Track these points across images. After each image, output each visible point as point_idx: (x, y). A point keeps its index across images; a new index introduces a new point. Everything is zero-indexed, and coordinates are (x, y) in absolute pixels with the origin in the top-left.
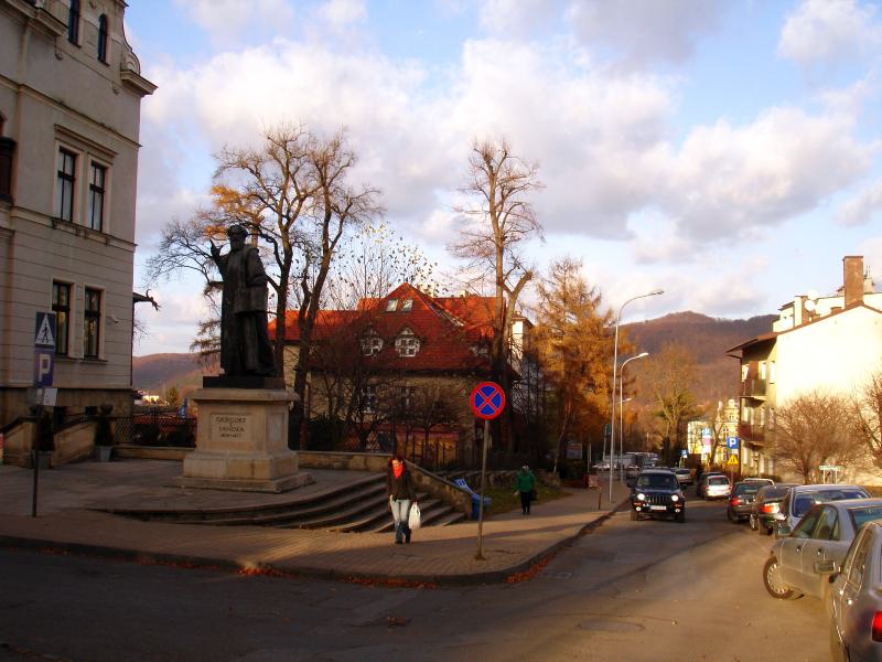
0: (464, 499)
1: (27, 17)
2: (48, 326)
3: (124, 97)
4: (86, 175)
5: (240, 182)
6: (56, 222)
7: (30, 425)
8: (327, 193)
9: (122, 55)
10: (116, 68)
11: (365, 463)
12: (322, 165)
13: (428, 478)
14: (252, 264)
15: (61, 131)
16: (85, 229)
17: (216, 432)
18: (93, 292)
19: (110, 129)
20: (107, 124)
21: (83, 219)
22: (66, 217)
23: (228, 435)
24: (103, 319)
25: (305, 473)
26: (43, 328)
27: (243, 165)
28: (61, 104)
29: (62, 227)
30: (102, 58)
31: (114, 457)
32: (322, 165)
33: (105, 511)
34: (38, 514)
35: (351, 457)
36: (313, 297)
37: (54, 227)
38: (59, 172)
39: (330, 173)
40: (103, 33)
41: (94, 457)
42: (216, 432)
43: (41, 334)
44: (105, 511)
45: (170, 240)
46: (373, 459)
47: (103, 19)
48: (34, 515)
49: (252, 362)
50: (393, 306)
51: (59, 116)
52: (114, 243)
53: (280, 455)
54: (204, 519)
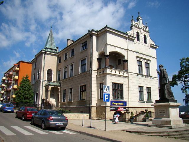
2: (107, 89)
6: (137, 74)
15: (137, 57)
19: (149, 56)
22: (141, 73)
23: (161, 114)
26: (106, 89)
33: (124, 131)
48: (83, 125)
49: (167, 96)
52: (152, 78)
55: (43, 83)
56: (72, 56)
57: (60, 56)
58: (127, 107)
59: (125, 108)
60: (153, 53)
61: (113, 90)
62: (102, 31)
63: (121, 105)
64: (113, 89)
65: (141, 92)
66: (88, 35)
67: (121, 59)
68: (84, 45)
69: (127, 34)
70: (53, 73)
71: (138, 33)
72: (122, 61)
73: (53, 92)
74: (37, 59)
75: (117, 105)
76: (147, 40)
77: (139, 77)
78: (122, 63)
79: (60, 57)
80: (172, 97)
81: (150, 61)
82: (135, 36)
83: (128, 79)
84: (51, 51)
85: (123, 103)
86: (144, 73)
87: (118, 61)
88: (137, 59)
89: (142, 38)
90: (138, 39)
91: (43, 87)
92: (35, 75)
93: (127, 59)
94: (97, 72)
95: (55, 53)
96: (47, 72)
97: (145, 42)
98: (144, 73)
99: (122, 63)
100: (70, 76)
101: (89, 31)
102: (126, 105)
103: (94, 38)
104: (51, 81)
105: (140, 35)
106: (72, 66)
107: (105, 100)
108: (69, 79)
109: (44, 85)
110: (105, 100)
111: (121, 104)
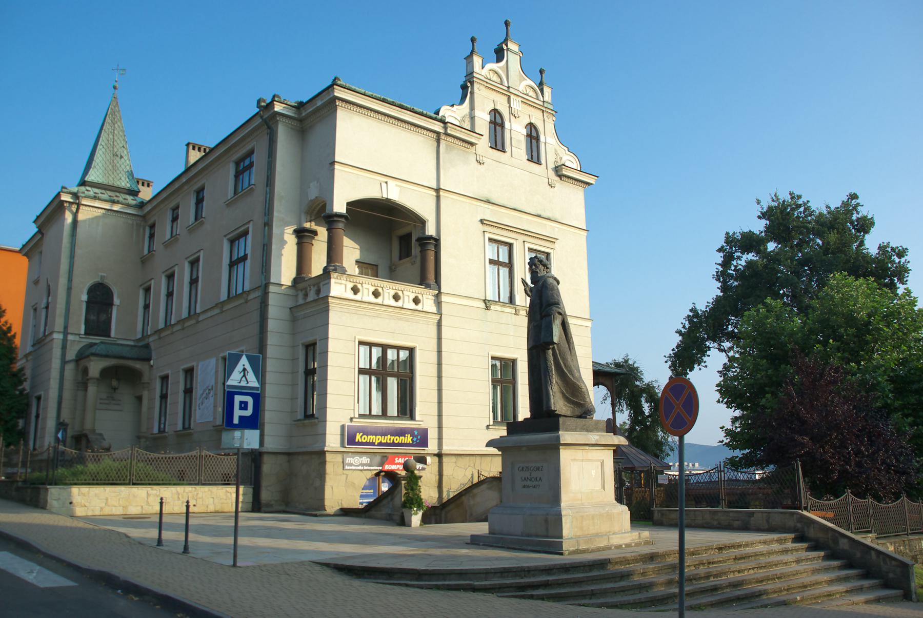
1: (438, 133)
11: (768, 521)
13: (846, 541)
22: (505, 297)
23: (528, 487)
26: (239, 367)
29: (498, 308)
34: (238, 564)
37: (487, 308)
48: (235, 565)
51: (488, 212)
55: (64, 348)
56: (196, 219)
57: (150, 222)
60: (571, 203)
61: (495, 388)
64: (493, 381)
66: (259, 121)
69: (443, 122)
70: (116, 301)
74: (43, 234)
75: (380, 444)
81: (552, 240)
85: (413, 435)
87: (399, 241)
90: (498, 143)
91: (64, 362)
92: (35, 310)
94: (589, 324)
96: (85, 297)
97: (534, 156)
99: (415, 250)
100: (185, 314)
101: (259, 101)
103: (283, 135)
104: (109, 336)
106: (194, 263)
107: (236, 421)
108: (183, 329)
109: (71, 355)
110: (236, 421)
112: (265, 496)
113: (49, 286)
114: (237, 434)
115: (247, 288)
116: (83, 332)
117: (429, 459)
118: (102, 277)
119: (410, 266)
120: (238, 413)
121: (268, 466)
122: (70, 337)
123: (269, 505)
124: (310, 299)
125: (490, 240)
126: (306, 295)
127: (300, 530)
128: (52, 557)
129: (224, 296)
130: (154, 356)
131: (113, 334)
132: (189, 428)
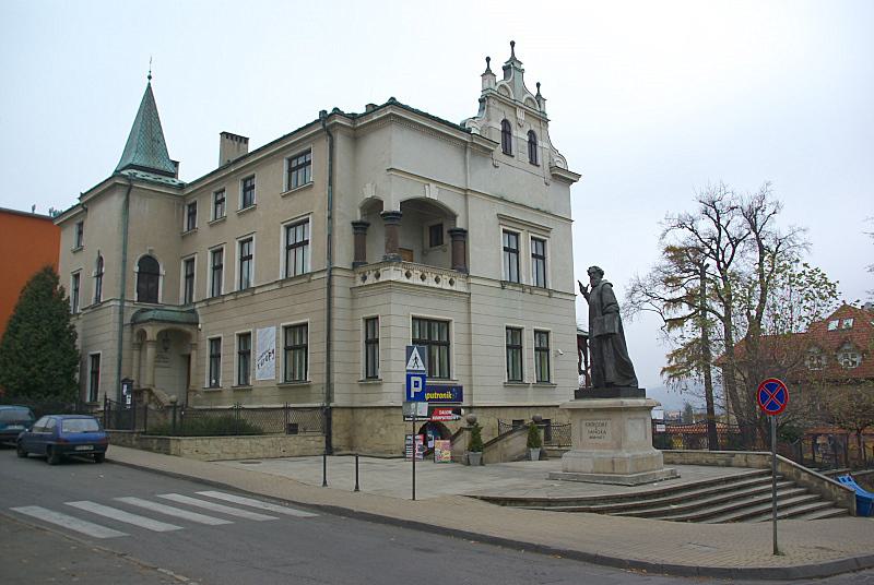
0: (845, 495)
2: (418, 356)
3: (555, 187)
4: (526, 248)
5: (680, 238)
6: (503, 284)
7: (467, 433)
8: (759, 240)
9: (550, 156)
10: (547, 168)
12: (751, 216)
13: (806, 474)
14: (606, 295)
16: (530, 287)
17: (586, 436)
18: (541, 335)
20: (542, 208)
21: (528, 279)
22: (515, 280)
24: (552, 353)
25: (668, 469)
26: (413, 357)
27: (682, 225)
28: (502, 199)
29: (510, 287)
30: (533, 161)
31: (542, 456)
32: (751, 216)
33: (475, 497)
35: (734, 455)
36: (755, 323)
38: (505, 249)
39: (759, 221)
40: (532, 143)
41: (528, 458)
42: (586, 436)
43: (411, 362)
44: (475, 497)
45: (634, 291)
46: (754, 458)
47: (531, 133)
49: (611, 375)
50: (833, 325)
52: (554, 295)
53: (640, 453)
54: (549, 506)
56: (244, 206)
58: (465, 408)
59: (457, 411)
62: (375, 118)
63: (443, 400)
65: (514, 348)
67: (441, 225)
68: (299, 167)
70: (162, 271)
71: (505, 122)
72: (445, 233)
73: (166, 349)
74: (86, 210)
76: (539, 149)
77: (509, 293)
78: (445, 241)
79: (189, 206)
80: (629, 378)
81: (548, 230)
82: (498, 138)
83: (469, 303)
84: (151, 177)
86: (528, 278)
88: (502, 227)
89: (522, 143)
90: (507, 151)
93: (465, 229)
95: (169, 186)
96: (137, 269)
98: (528, 278)
99: (447, 240)
102: (460, 399)
105: (514, 133)
109: (127, 320)
111: (442, 396)
112: (335, 442)
113: (101, 258)
114: (413, 405)
115: (309, 269)
116: (136, 299)
117: (463, 411)
118: (150, 251)
119: (444, 255)
120: (413, 390)
121: (336, 418)
122: (126, 304)
123: (337, 450)
124: (368, 282)
125: (504, 231)
126: (364, 278)
127: (41, 435)
128: (294, 502)
129: (281, 276)
130: (201, 320)
131: (160, 301)
132: (247, 384)
